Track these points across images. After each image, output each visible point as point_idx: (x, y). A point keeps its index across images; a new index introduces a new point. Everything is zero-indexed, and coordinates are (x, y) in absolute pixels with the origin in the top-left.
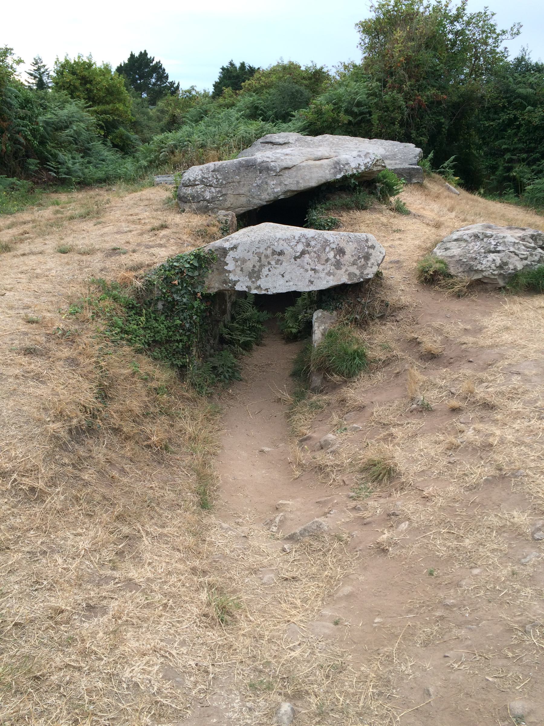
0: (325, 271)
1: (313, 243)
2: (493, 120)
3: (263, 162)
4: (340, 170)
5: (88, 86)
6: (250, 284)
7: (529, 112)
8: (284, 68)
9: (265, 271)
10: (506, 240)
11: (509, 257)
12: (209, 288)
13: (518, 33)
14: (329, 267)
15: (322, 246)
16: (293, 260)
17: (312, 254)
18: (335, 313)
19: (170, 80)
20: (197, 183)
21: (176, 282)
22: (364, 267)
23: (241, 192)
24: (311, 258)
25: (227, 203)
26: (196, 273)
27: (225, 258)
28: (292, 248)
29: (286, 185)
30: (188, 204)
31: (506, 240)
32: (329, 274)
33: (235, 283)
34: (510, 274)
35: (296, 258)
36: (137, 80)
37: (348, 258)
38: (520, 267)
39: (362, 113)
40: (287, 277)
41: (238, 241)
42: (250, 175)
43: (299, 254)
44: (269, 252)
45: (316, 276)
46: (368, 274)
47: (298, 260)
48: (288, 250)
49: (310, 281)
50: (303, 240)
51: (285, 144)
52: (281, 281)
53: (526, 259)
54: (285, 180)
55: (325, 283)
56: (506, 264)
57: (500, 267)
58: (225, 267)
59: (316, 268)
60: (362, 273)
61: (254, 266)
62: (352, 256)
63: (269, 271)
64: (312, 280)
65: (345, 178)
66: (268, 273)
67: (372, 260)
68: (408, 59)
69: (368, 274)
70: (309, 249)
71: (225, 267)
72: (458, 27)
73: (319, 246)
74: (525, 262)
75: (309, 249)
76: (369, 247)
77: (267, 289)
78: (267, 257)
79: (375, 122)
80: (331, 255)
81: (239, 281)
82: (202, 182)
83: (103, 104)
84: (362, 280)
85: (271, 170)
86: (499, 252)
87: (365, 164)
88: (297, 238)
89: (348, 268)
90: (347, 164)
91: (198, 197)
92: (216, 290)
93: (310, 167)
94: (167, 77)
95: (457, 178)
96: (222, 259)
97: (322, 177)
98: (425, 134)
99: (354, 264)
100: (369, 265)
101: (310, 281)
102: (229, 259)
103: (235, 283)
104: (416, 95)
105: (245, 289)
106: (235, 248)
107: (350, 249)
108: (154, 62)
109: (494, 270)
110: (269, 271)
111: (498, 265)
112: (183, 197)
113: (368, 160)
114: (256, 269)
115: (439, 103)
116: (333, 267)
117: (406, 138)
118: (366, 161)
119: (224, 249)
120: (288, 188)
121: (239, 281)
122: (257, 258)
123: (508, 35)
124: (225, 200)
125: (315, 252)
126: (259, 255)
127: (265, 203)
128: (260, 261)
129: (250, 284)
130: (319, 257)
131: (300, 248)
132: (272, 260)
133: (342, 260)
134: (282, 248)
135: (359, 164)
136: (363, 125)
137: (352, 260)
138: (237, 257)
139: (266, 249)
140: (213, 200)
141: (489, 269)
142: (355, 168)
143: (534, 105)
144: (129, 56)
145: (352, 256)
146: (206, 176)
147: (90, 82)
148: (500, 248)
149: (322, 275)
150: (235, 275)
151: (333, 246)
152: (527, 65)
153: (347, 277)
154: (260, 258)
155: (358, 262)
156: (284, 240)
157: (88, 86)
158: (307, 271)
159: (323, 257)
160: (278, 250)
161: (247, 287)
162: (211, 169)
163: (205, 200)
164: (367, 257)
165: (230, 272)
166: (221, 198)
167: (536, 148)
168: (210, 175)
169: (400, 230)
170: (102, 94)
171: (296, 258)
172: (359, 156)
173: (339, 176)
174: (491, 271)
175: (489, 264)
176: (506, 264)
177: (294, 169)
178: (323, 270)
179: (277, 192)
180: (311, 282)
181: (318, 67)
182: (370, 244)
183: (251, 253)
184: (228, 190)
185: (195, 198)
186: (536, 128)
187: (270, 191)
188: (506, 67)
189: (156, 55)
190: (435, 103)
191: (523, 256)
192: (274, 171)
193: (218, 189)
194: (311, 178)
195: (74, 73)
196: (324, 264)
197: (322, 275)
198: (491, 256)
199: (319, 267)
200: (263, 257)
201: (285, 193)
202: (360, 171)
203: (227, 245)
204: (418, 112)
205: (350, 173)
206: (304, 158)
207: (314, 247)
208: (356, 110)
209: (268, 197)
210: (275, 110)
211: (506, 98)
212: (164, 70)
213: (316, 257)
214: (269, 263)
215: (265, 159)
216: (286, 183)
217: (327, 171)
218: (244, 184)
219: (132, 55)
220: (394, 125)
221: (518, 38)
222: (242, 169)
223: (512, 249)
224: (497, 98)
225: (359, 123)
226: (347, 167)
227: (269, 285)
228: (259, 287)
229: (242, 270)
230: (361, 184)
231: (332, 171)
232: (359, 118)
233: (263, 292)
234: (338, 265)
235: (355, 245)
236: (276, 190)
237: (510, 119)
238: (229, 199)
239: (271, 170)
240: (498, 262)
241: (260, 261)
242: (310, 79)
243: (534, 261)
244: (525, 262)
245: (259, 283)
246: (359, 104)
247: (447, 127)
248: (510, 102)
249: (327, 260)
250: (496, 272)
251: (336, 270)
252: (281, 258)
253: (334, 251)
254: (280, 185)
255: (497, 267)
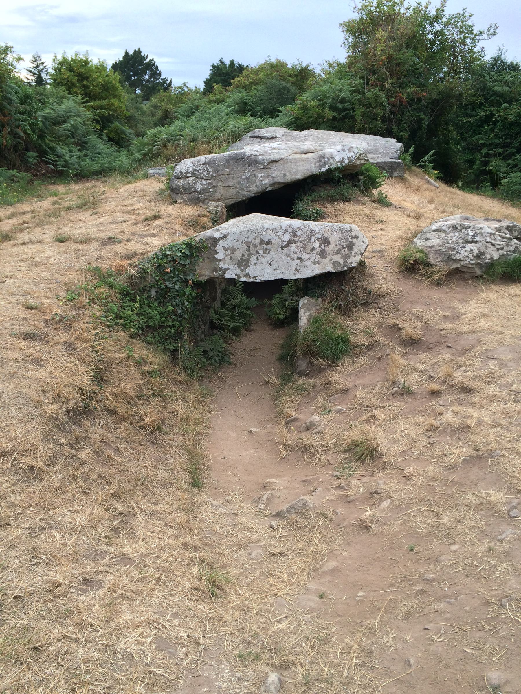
0: (311, 260)
1: (299, 233)
2: (471, 116)
3: (251, 155)
4: (325, 164)
5: (85, 82)
6: (239, 272)
7: (505, 109)
8: (272, 66)
9: (253, 259)
10: (482, 231)
11: (486, 247)
12: (200, 276)
13: (494, 34)
14: (314, 256)
15: (308, 236)
16: (280, 249)
17: (299, 243)
18: (320, 300)
19: (162, 77)
20: (188, 175)
21: (169, 270)
22: (348, 256)
23: (231, 184)
24: (297, 248)
25: (217, 195)
26: (188, 262)
27: (215, 247)
28: (279, 238)
29: (273, 177)
30: (180, 196)
31: (482, 231)
32: (314, 262)
33: (225, 271)
34: (486, 263)
35: (282, 247)
36: (131, 76)
37: (332, 247)
38: (496, 256)
39: (345, 109)
40: (274, 265)
41: (228, 231)
42: (239, 167)
43: (285, 243)
44: (257, 241)
45: (302, 264)
46: (351, 263)
47: (285, 249)
48: (276, 240)
49: (296, 269)
50: (290, 230)
51: (273, 138)
52: (269, 270)
53: (502, 249)
54: (272, 173)
55: (310, 271)
56: (483, 253)
57: (478, 257)
58: (216, 256)
59: (302, 256)
60: (346, 262)
61: (243, 255)
62: (337, 245)
63: (258, 259)
64: (298, 268)
65: (329, 171)
66: (256, 261)
67: (355, 250)
68: (390, 58)
69: (351, 263)
70: (296, 239)
71: (216, 256)
72: (437, 27)
73: (305, 236)
74: (501, 252)
75: (296, 239)
76: (352, 237)
77: (255, 277)
78: (255, 246)
79: (359, 118)
80: (317, 244)
81: (228, 269)
82: (193, 174)
83: (99, 99)
84: (346, 268)
85: (260, 163)
86: (476, 242)
87: (349, 158)
88: (284, 228)
89: (333, 257)
90: (332, 157)
91: (190, 188)
92: (207, 278)
93: (296, 161)
94: (160, 74)
95: (437, 172)
96: (213, 248)
97: (308, 170)
98: (405, 130)
99: (338, 253)
100: (353, 254)
101: (296, 269)
102: (219, 248)
103: (225, 271)
104: (397, 92)
105: (234, 277)
106: (225, 237)
107: (334, 238)
108: (148, 60)
109: (471, 260)
110: (258, 259)
111: (475, 254)
112: (176, 188)
113: (352, 154)
114: (245, 258)
115: (419, 100)
116: (318, 256)
117: (387, 133)
118: (349, 155)
119: (215, 238)
120: (275, 180)
121: (228, 269)
122: (246, 247)
123: (485, 36)
124: (215, 192)
125: (301, 242)
126: (248, 244)
127: (253, 195)
128: (248, 250)
129: (239, 272)
130: (304, 246)
131: (287, 237)
132: (260, 249)
133: (326, 249)
134: (269, 238)
135: (343, 158)
136: (347, 120)
137: (336, 249)
138: (227, 246)
139: (254, 239)
140: (204, 191)
141: (466, 258)
142: (339, 162)
143: (510, 102)
144: (124, 54)
145: (337, 245)
146: (197, 169)
147: (87, 78)
148: (477, 239)
149: (308, 264)
150: (225, 264)
151: (319, 236)
152: (503, 64)
153: (332, 266)
154: (249, 247)
155: (342, 251)
156: (272, 230)
157: (85, 82)
158: (293, 259)
159: (309, 246)
160: (266, 239)
161: (236, 275)
162: (202, 162)
163: (196, 191)
164: (351, 247)
165: (220, 260)
166: (211, 190)
167: (511, 143)
168: (201, 168)
169: (382, 221)
170: (98, 90)
171: (282, 247)
172: (343, 150)
173: (324, 169)
174: (469, 260)
175: (467, 254)
176: (483, 253)
177: (281, 162)
178: (309, 259)
179: (265, 184)
180: (298, 271)
181: (304, 65)
182: (353, 234)
183: (240, 242)
184: (218, 182)
185: (187, 190)
186: (512, 124)
187: (258, 183)
188: (483, 66)
189: (150, 53)
190: (415, 100)
191: (499, 247)
192: (262, 164)
193: (208, 181)
194: (297, 171)
195: (71, 70)
196: (310, 253)
197: (308, 264)
198: (469, 246)
199: (305, 256)
200: (251, 246)
201: (273, 185)
202: (344, 164)
203: (217, 235)
204: (399, 108)
205: (335, 166)
206: (290, 152)
207: (300, 237)
208: (340, 106)
209: (256, 189)
210: (263, 106)
211: (483, 95)
212: (157, 67)
213: (302, 247)
214: (257, 252)
215: (254, 153)
216: (273, 175)
217: (313, 165)
218: (233, 177)
219: (127, 53)
220: (377, 120)
221: (494, 37)
222: (232, 162)
223: (488, 240)
224: (474, 96)
225: (343, 119)
226: (331, 161)
227: (258, 273)
228: (247, 275)
229: (231, 259)
230: (345, 177)
231: (318, 164)
232: (344, 114)
233: (252, 280)
234: (323, 254)
235: (340, 235)
236: (263, 182)
237: (486, 116)
238: (219, 191)
239: (260, 163)
240: (476, 252)
241: (248, 250)
242: (296, 76)
243: (509, 251)
244: (501, 252)
245: (247, 271)
246: (343, 101)
247: (427, 123)
248: (486, 99)
249: (313, 249)
250: (473, 262)
251: (321, 259)
252: (268, 247)
253: (319, 241)
254: (268, 177)
255: (474, 257)
